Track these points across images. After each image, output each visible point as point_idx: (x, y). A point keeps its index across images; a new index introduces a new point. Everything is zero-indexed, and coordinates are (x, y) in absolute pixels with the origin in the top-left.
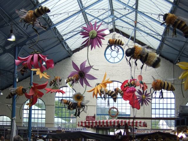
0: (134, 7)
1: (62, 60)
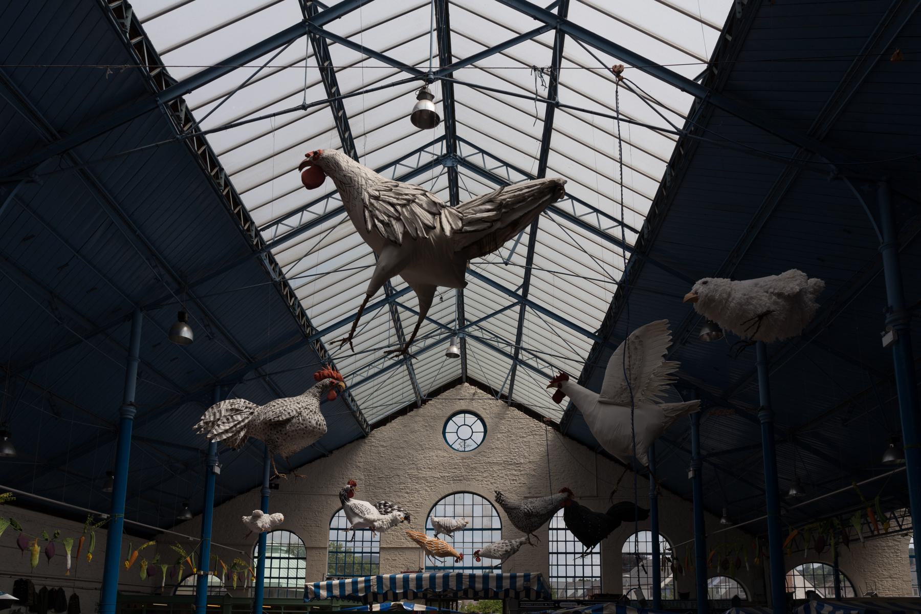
0: (520, 292)
1: (345, 445)
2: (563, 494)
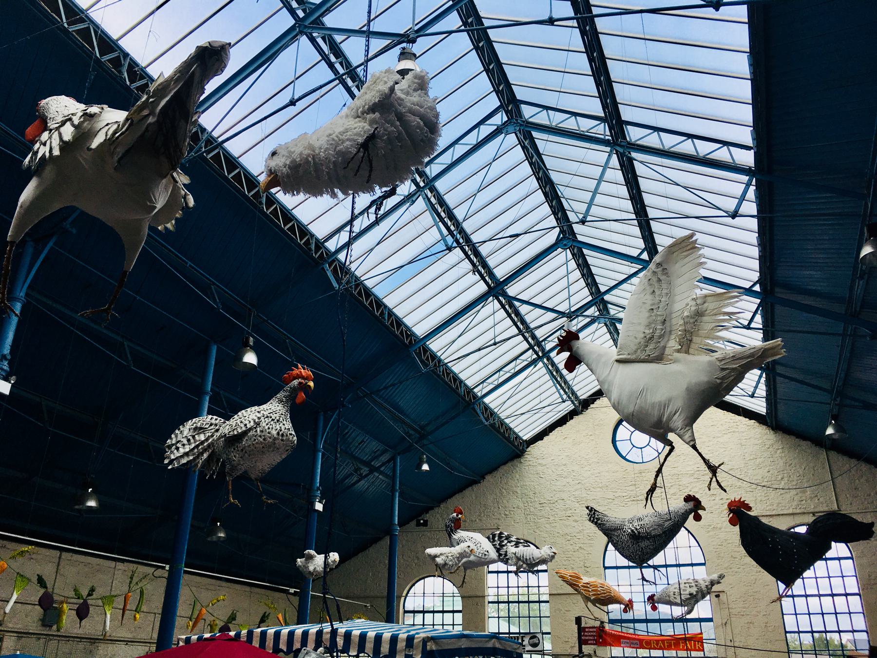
2: (687, 504)
